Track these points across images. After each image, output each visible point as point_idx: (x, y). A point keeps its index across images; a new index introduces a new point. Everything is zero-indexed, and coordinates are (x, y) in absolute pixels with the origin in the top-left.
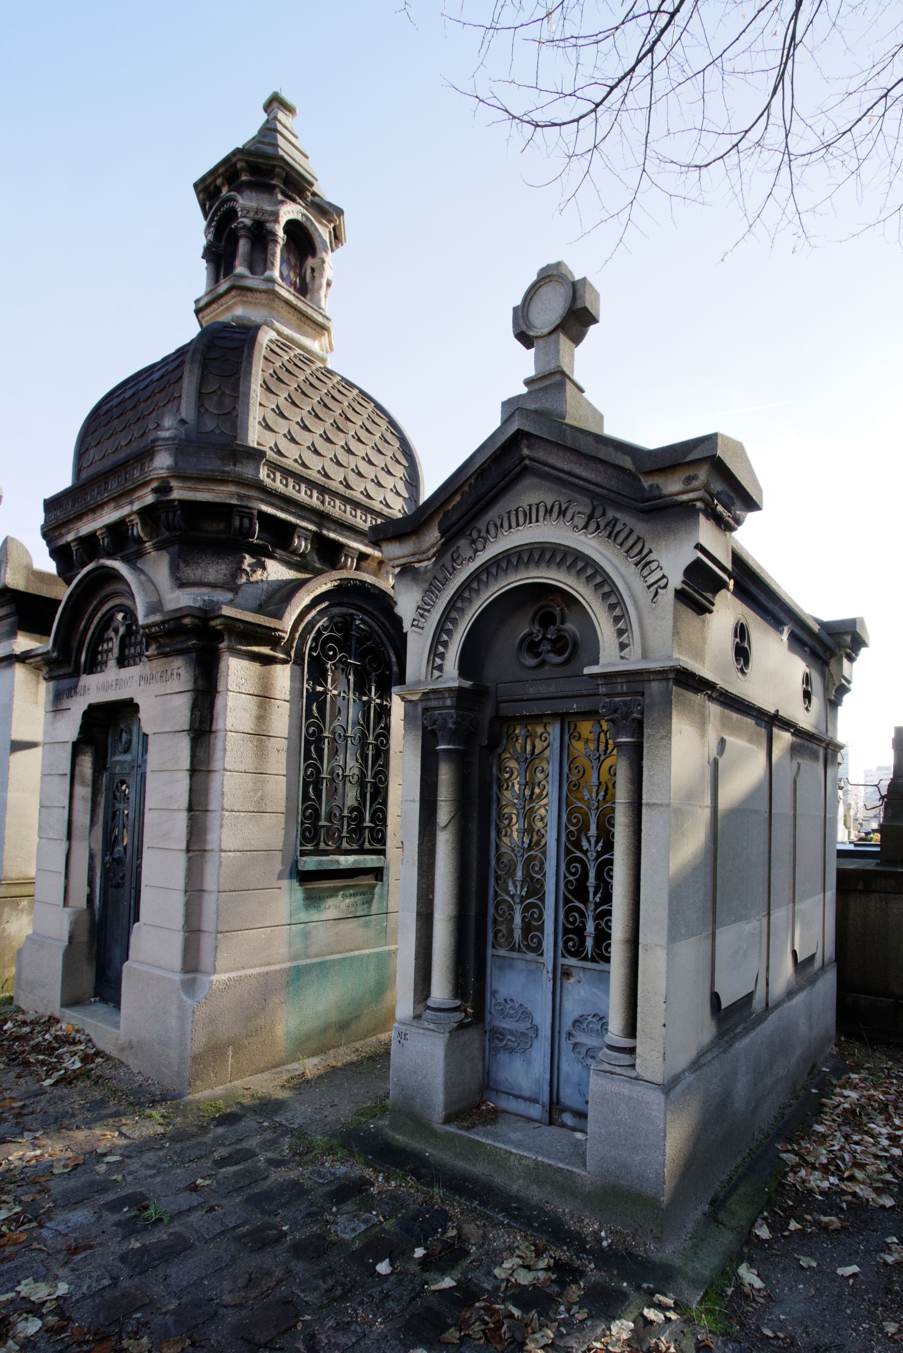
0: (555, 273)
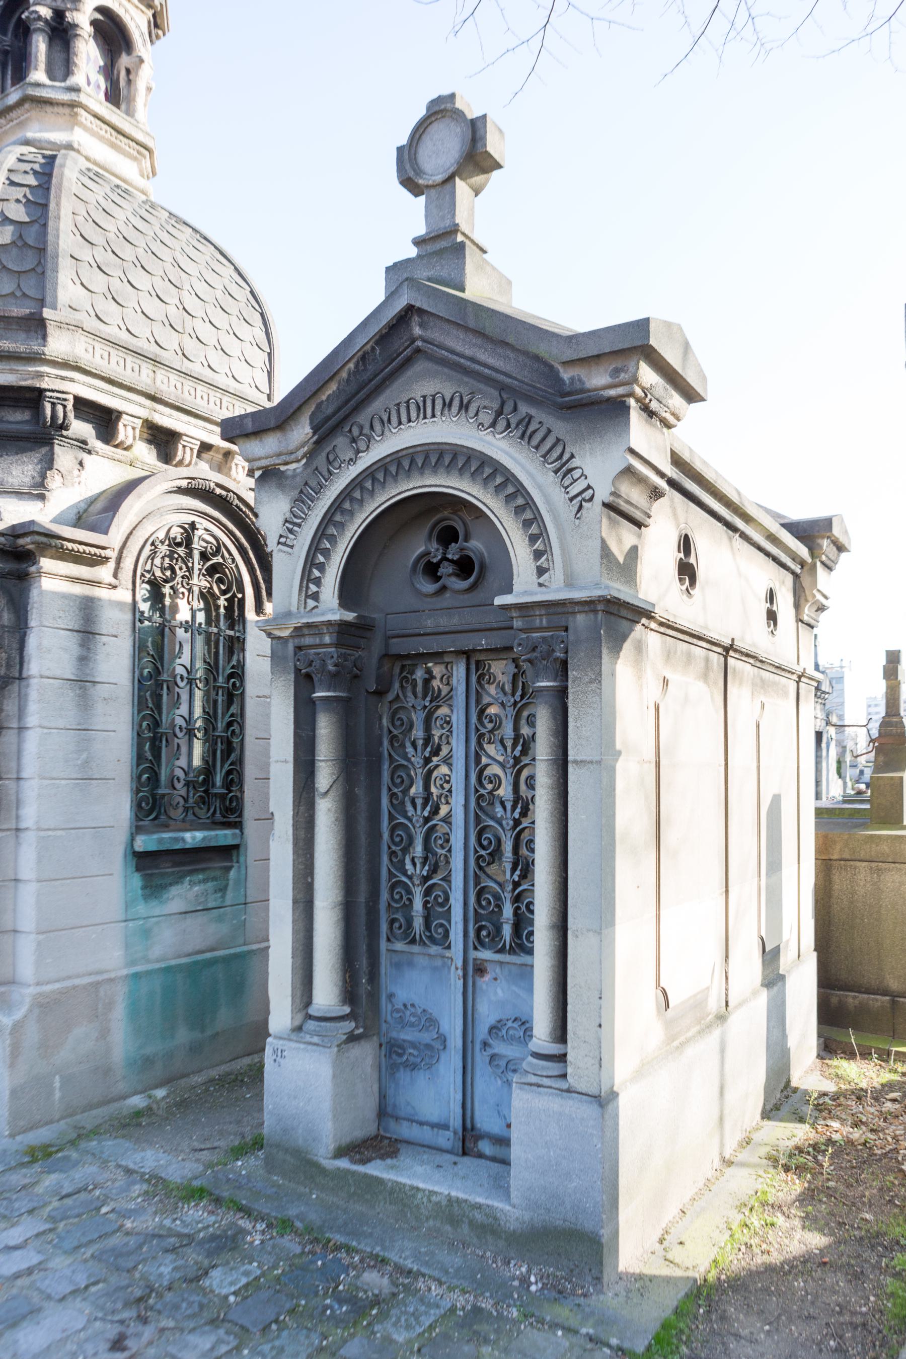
0: (449, 106)
